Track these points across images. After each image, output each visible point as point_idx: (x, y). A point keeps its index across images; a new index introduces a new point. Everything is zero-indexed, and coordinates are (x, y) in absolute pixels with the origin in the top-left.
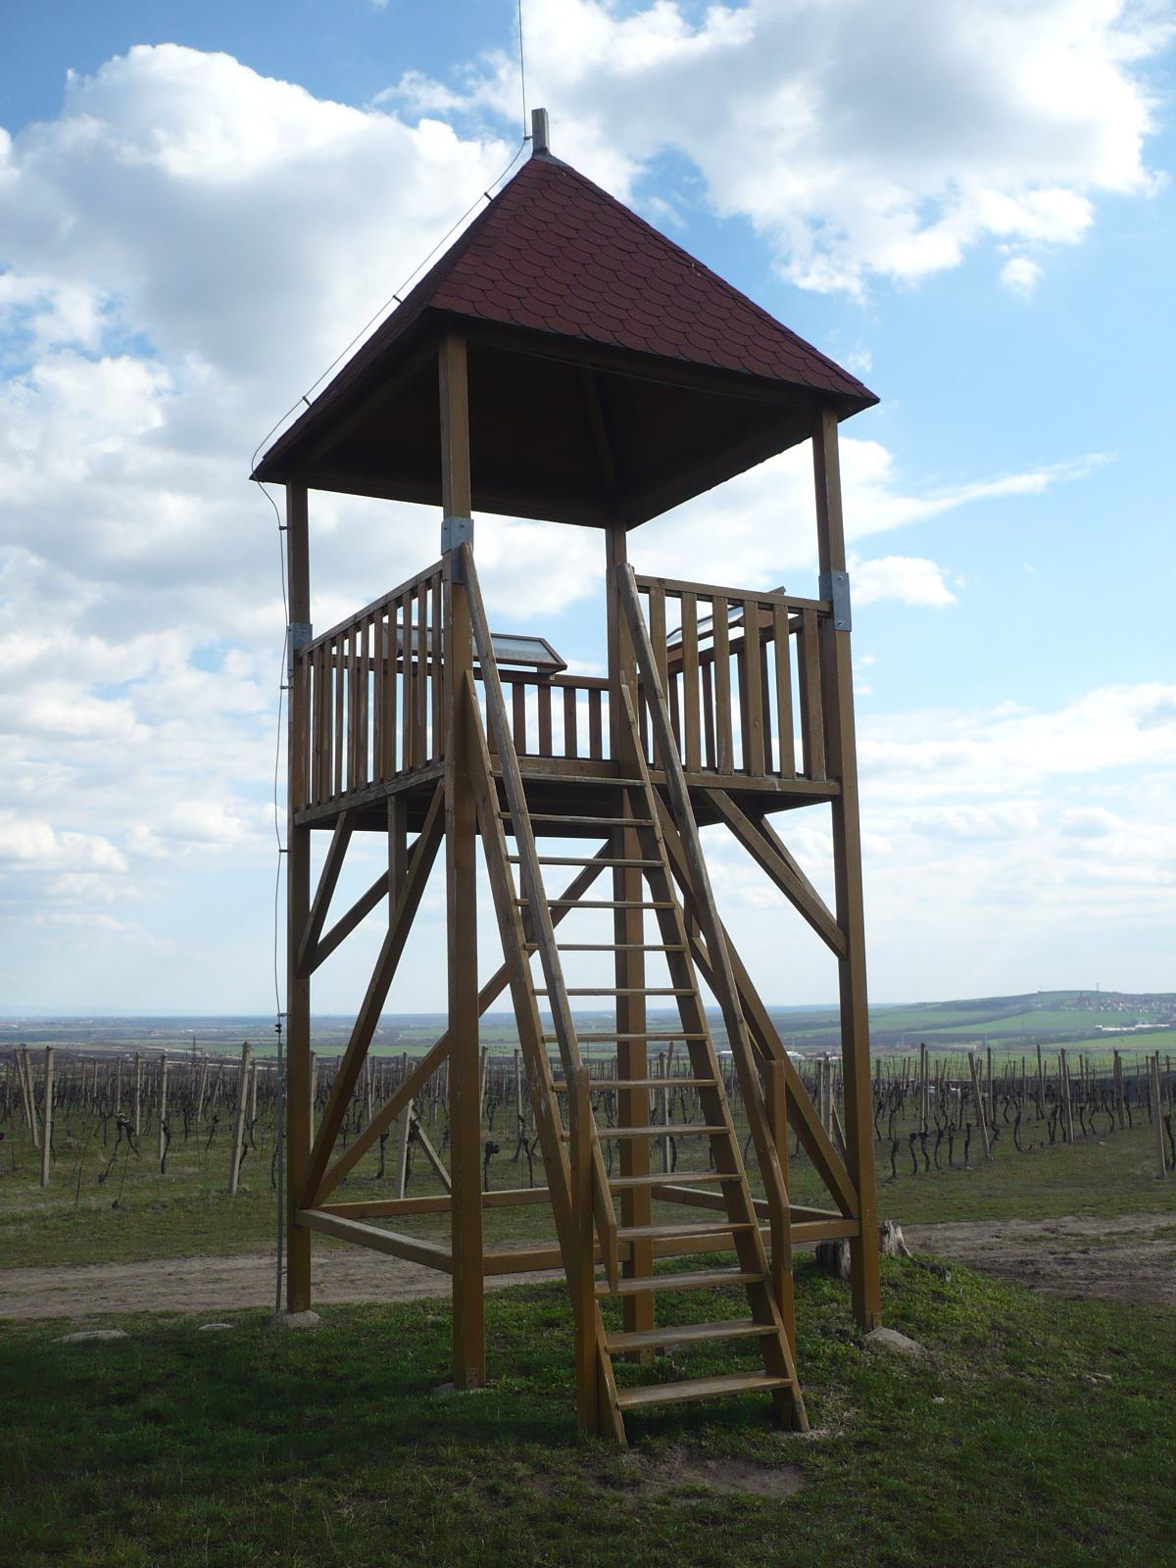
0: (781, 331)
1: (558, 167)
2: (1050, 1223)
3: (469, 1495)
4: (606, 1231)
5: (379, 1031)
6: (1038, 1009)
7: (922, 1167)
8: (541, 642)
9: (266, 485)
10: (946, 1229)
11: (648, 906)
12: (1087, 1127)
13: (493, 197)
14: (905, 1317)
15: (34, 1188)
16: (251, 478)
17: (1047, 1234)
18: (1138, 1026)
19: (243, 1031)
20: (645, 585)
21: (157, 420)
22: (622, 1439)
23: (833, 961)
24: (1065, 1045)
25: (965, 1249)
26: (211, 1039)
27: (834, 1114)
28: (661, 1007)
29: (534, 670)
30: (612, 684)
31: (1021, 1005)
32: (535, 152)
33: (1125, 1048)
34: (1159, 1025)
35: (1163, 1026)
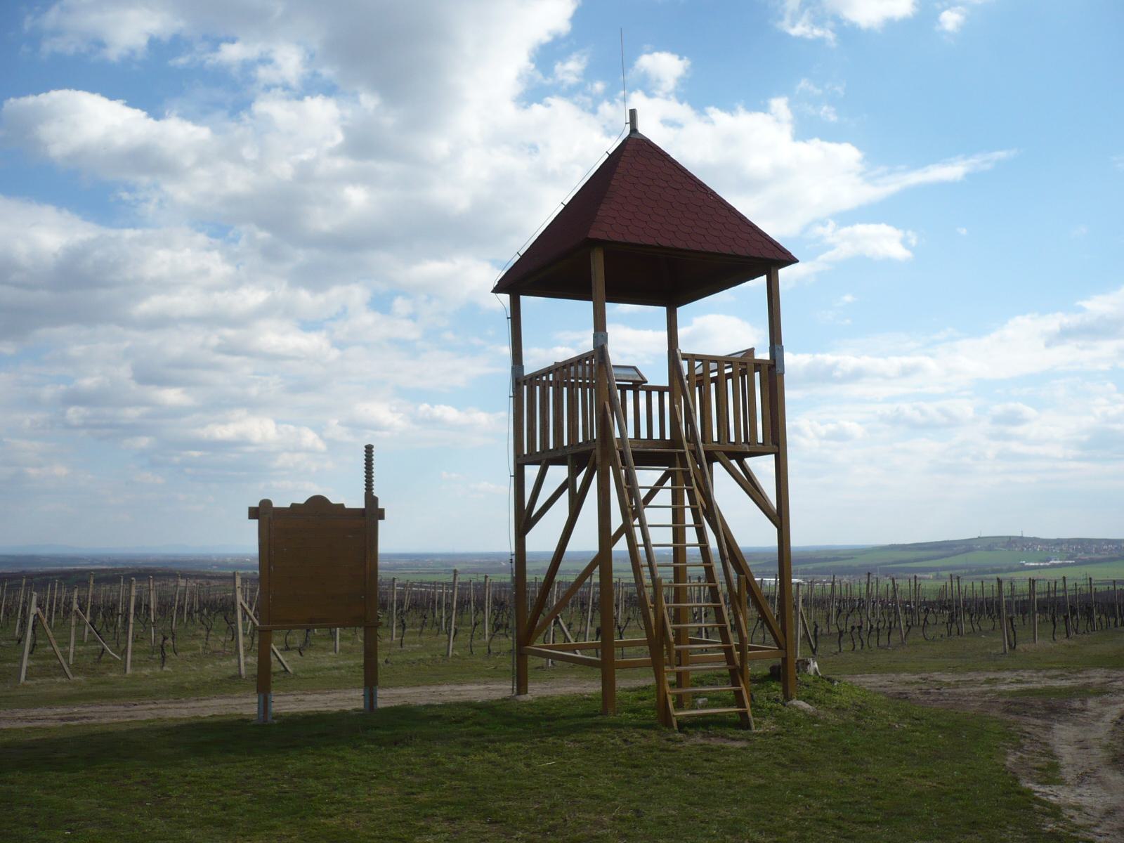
0: (751, 227)
1: (643, 140)
2: (924, 675)
3: (618, 741)
4: (669, 644)
5: (564, 559)
6: (978, 549)
7: (858, 647)
8: (635, 368)
9: (499, 295)
10: (862, 677)
11: (687, 507)
12: (976, 627)
13: (610, 153)
14: (810, 698)
15: (332, 654)
16: (493, 292)
17: (921, 681)
18: (1051, 562)
19: (490, 560)
20: (685, 357)
21: (340, 138)
22: (676, 728)
23: (775, 530)
24: (1001, 576)
25: (871, 687)
26: (386, 569)
27: (801, 612)
28: (693, 552)
29: (631, 383)
30: (669, 388)
31: (967, 546)
32: (631, 131)
33: (1042, 578)
34: (1067, 562)
35: (1070, 562)
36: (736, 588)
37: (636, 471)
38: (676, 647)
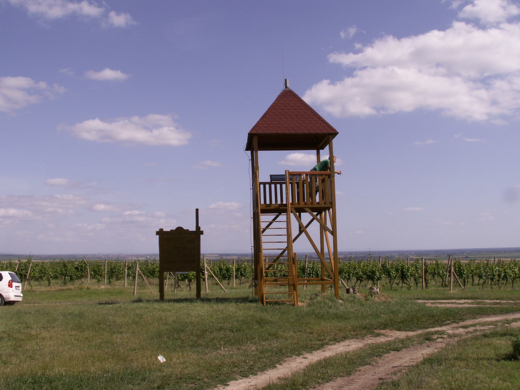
0: (323, 121)
36: (343, 256)
37: (261, 216)
38: (265, 278)
